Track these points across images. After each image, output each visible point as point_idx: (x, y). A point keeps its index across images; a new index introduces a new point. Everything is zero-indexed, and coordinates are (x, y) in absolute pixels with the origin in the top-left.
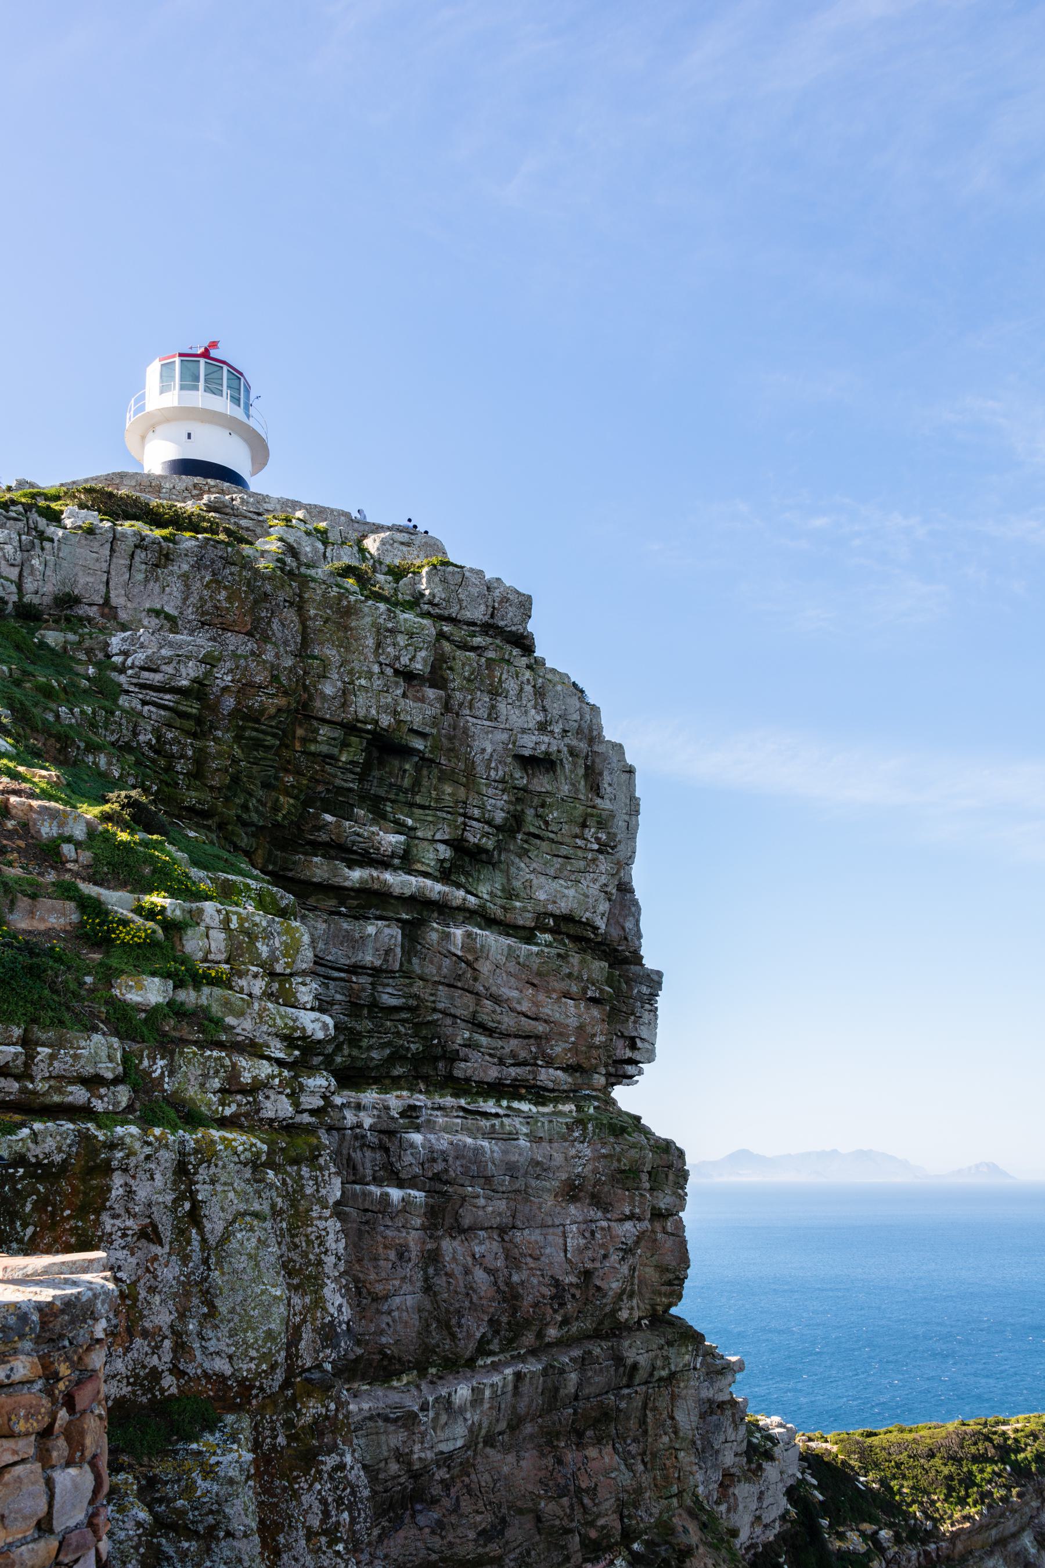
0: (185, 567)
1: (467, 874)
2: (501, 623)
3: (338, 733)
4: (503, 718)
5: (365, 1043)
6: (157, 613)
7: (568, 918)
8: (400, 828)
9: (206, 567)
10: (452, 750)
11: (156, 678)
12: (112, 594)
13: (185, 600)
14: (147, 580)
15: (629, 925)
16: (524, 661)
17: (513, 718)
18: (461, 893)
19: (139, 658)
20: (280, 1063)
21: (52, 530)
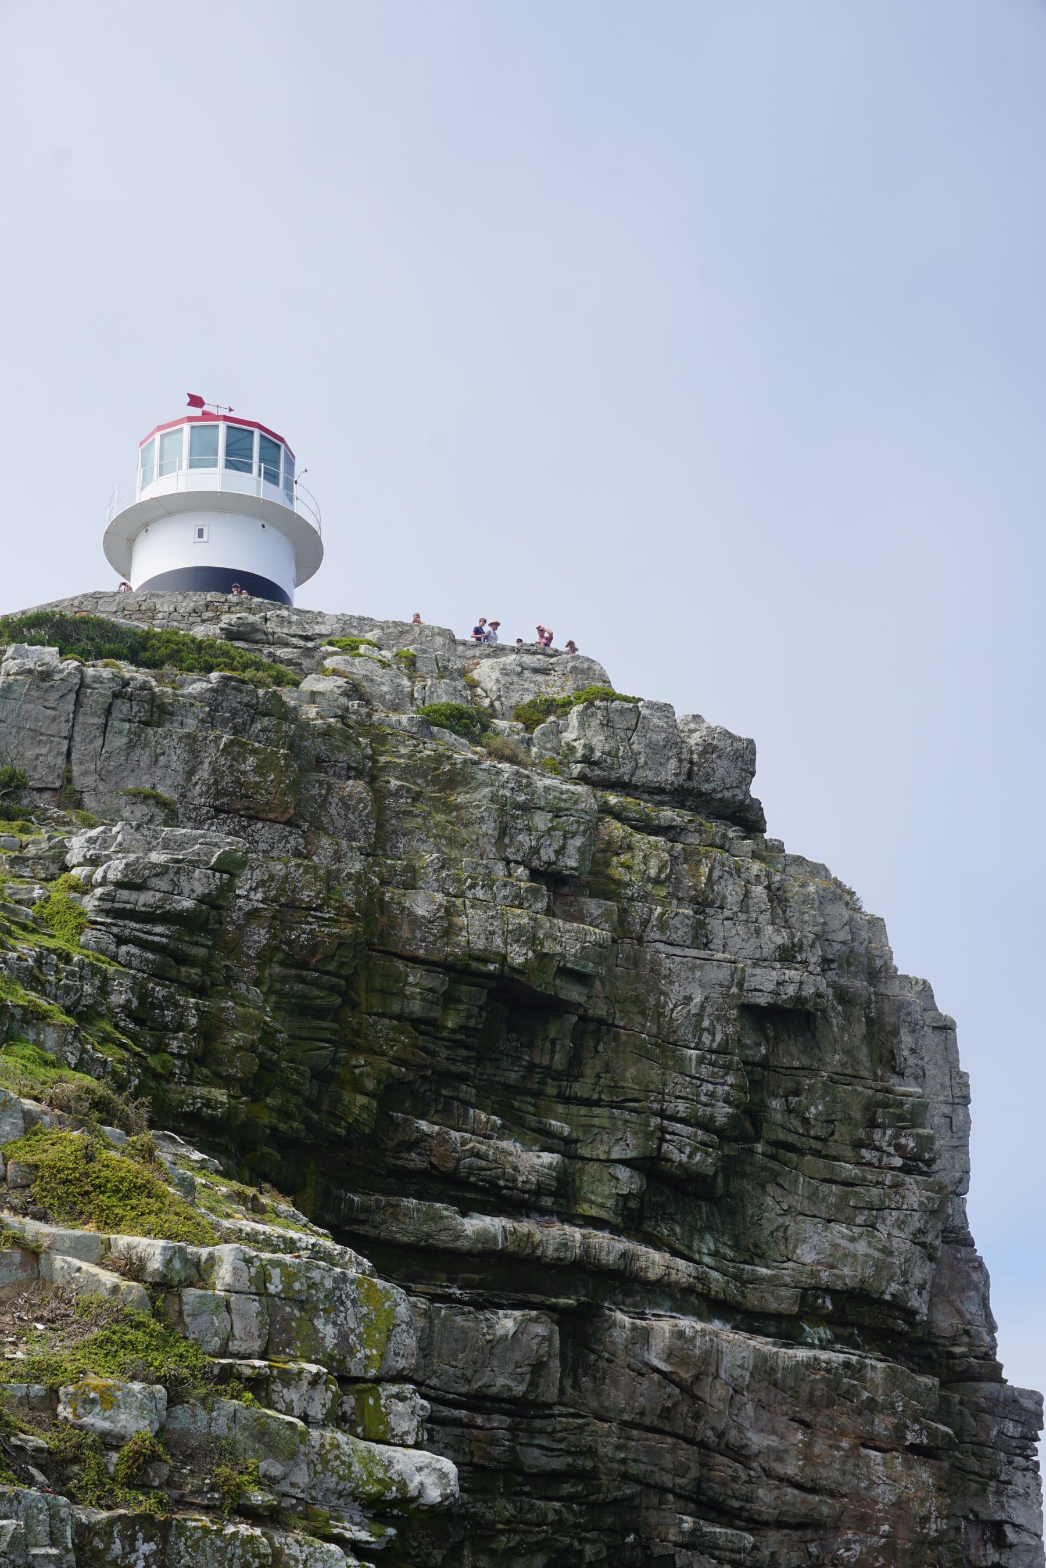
0: (191, 724)
2: (706, 787)
3: (438, 981)
4: (718, 943)
8: (547, 1140)
9: (224, 722)
11: (143, 899)
12: (76, 769)
14: (131, 746)
17: (736, 943)
19: (115, 868)
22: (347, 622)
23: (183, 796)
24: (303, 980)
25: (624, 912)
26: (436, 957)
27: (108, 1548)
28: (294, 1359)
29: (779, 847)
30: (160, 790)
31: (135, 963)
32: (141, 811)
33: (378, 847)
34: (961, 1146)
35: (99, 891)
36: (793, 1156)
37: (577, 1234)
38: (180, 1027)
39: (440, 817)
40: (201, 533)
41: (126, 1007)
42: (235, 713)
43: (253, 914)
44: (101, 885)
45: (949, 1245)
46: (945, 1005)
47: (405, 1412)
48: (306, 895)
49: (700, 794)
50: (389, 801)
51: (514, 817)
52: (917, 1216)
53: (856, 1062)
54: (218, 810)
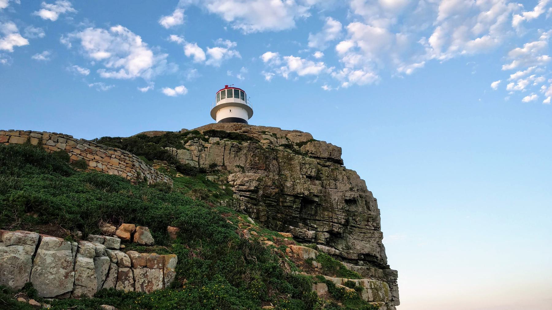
0: (245, 151)
1: (335, 242)
2: (333, 157)
3: (292, 199)
4: (338, 188)
6: (238, 166)
7: (368, 255)
8: (313, 229)
10: (325, 200)
11: (244, 188)
12: (225, 162)
13: (246, 161)
14: (235, 156)
15: (382, 255)
17: (342, 188)
18: (333, 249)
19: (239, 182)
21: (206, 145)
33: (279, 174)
35: (236, 186)
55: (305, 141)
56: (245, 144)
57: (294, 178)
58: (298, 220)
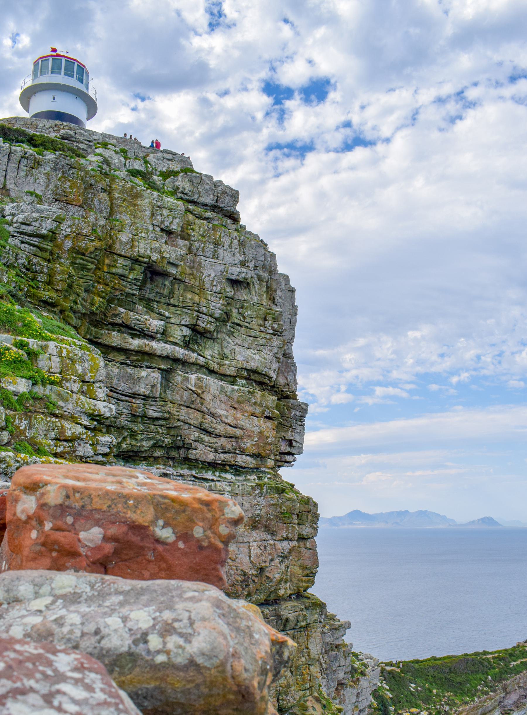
0: (48, 169)
1: (199, 344)
3: (128, 263)
5: (139, 437)
9: (59, 169)
10: (192, 274)
11: (29, 229)
12: (8, 182)
14: (27, 175)
16: (234, 226)
17: (227, 258)
18: (195, 355)
19: (21, 217)
20: (86, 428)
22: (103, 135)
23: (44, 194)
24: (83, 259)
25: (191, 245)
26: (128, 255)
27: (14, 421)
28: (69, 375)
29: (244, 227)
30: (37, 191)
31: (27, 250)
32: (30, 198)
34: (293, 329)
35: (15, 225)
36: (239, 328)
37: (168, 346)
38: (41, 272)
39: (132, 208)
40: (54, 98)
41: (23, 264)
42: (63, 166)
43: (66, 236)
44: (16, 223)
45: (286, 358)
46: (293, 284)
47: (101, 393)
48: (85, 231)
49: (220, 208)
50: (115, 201)
51: (157, 210)
52: (275, 348)
53: (262, 300)
54: (56, 200)
55: (176, 169)
56: (50, 156)
57: (136, 229)
58: (136, 300)
